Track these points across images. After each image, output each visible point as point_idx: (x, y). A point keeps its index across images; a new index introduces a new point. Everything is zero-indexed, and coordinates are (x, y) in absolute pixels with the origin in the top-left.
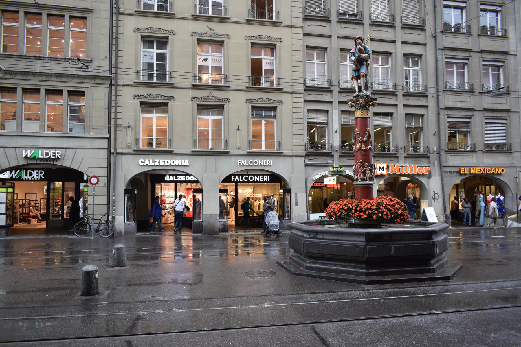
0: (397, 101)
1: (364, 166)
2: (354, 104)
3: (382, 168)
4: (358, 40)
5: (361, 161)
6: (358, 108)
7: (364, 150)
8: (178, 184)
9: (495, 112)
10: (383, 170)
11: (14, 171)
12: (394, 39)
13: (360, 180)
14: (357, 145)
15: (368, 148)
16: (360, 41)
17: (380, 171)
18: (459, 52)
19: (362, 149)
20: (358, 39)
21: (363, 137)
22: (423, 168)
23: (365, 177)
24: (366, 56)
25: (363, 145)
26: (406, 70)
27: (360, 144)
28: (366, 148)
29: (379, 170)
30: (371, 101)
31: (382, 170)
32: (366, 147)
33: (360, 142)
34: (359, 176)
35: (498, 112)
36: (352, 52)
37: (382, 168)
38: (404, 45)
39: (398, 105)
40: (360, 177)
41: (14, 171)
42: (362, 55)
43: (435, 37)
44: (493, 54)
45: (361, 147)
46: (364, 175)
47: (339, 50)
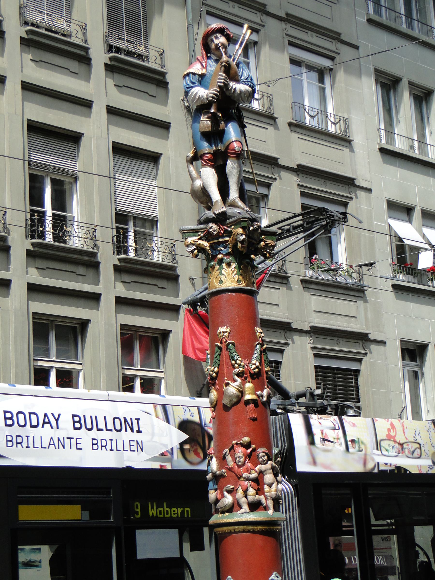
0: (97, 283)
1: (258, 457)
4: (216, 38)
5: (246, 439)
7: (253, 401)
8: (71, 439)
9: (336, 339)
11: (269, 245)
13: (246, 508)
14: (227, 384)
15: (262, 396)
16: (222, 40)
19: (248, 397)
20: (218, 35)
21: (248, 356)
23: (262, 497)
25: (249, 385)
27: (239, 380)
28: (258, 396)
32: (259, 393)
33: (238, 375)
34: (240, 493)
35: (341, 340)
36: (194, 74)
39: (103, 298)
40: (246, 496)
41: (269, 245)
42: (233, 85)
44: (323, 181)
45: (242, 393)
46: (259, 491)
47: (20, 86)
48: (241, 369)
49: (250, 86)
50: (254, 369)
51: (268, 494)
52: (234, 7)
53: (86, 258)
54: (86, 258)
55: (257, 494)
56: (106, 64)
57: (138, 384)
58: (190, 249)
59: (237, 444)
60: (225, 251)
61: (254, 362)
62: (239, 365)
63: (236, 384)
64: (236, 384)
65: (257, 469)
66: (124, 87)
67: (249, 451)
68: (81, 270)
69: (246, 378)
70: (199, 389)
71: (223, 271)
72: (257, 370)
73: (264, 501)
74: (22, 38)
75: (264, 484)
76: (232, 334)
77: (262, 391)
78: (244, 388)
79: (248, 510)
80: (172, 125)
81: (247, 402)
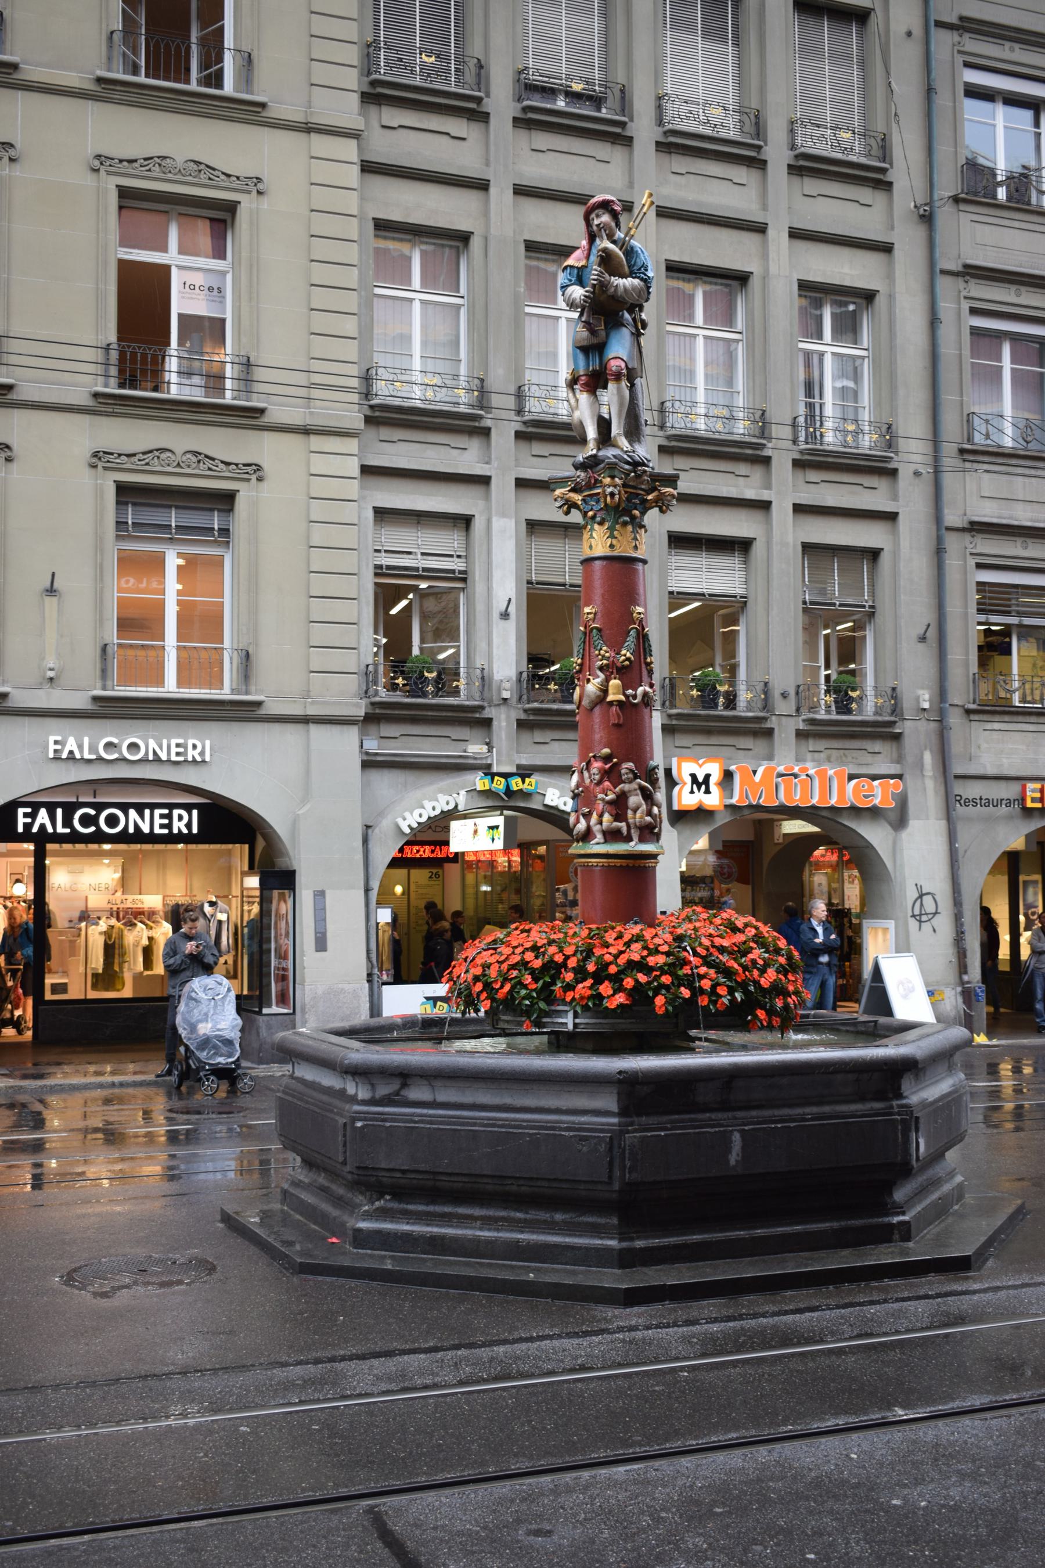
1: (620, 776)
2: (577, 498)
3: (700, 779)
4: (598, 216)
5: (606, 751)
6: (593, 517)
10: (708, 791)
12: (758, 217)
13: (599, 837)
15: (635, 697)
16: (606, 218)
17: (692, 792)
18: (1023, 289)
19: (610, 698)
20: (600, 211)
22: (876, 783)
24: (634, 288)
25: (615, 683)
26: (808, 355)
27: (602, 676)
29: (688, 788)
30: (654, 489)
31: (703, 787)
33: (601, 668)
36: (572, 267)
37: (700, 779)
38: (801, 245)
40: (600, 823)
43: (927, 219)
45: (605, 692)
48: (605, 662)
49: (642, 279)
50: (624, 661)
51: (631, 821)
52: (1012, 50)
53: (749, 452)
54: (749, 452)
55: (615, 820)
56: (789, 165)
57: (58, 747)
58: (558, 504)
59: (594, 757)
60: (596, 507)
61: (623, 652)
62: (603, 656)
63: (598, 680)
64: (598, 680)
65: (617, 789)
66: (820, 198)
67: (607, 766)
68: (742, 468)
69: (612, 673)
70: (923, 632)
71: (594, 535)
72: (627, 663)
73: (625, 830)
74: (658, 143)
75: (627, 808)
76: (599, 616)
77: (635, 689)
78: (607, 687)
79: (602, 841)
80: (896, 246)
81: (611, 703)
